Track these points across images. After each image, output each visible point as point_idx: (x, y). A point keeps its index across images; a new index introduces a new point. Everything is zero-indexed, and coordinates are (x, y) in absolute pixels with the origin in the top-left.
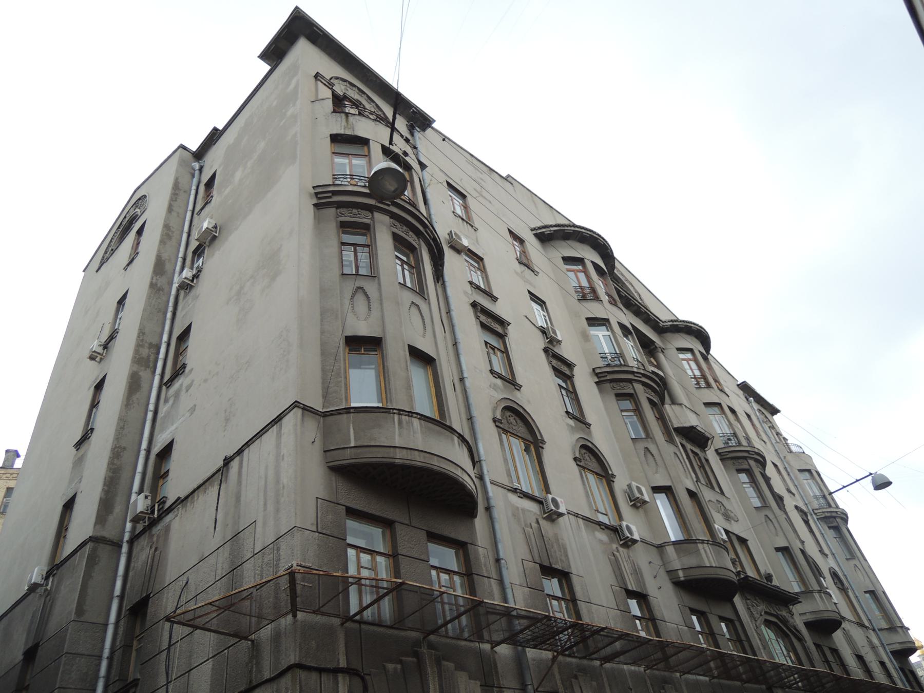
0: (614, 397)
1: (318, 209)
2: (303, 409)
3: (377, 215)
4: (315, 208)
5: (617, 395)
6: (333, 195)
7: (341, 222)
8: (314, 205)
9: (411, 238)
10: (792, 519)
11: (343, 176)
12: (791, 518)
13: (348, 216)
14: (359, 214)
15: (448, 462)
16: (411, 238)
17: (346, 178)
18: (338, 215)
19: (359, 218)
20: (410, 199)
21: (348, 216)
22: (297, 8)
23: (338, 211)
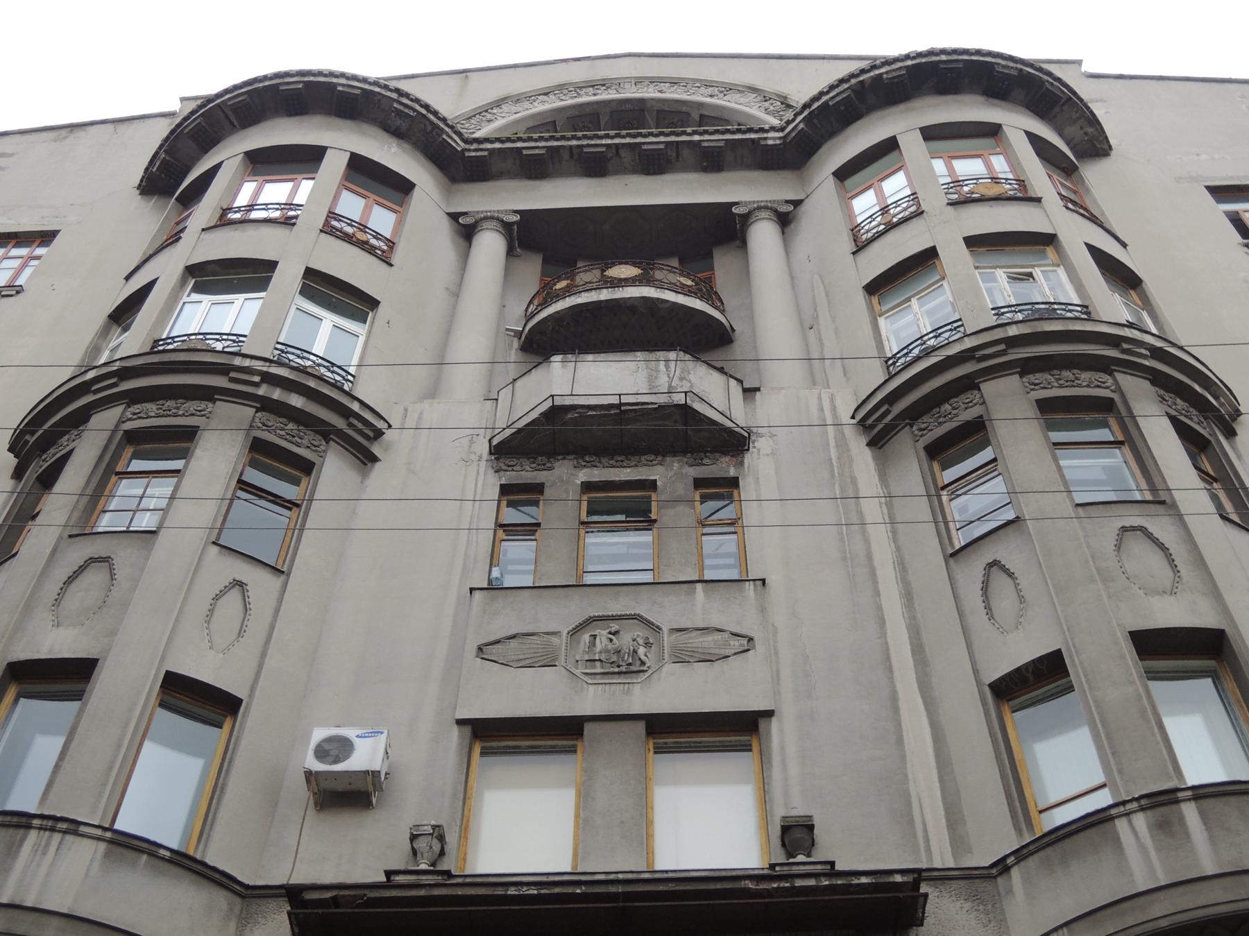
0: (1033, 412)
1: (880, 448)
2: (1196, 798)
3: (989, 388)
4: (873, 448)
5: (1045, 406)
6: (891, 404)
7: (927, 448)
8: (869, 444)
9: (1087, 385)
10: (971, 469)
11: (299, 352)
12: (969, 470)
13: (278, 434)
14: (954, 409)
15: (1154, 896)
16: (1087, 385)
17: (287, 352)
18: (916, 436)
19: (176, 415)
20: (1128, 321)
21: (278, 434)
22: (180, 98)
23: (915, 428)
